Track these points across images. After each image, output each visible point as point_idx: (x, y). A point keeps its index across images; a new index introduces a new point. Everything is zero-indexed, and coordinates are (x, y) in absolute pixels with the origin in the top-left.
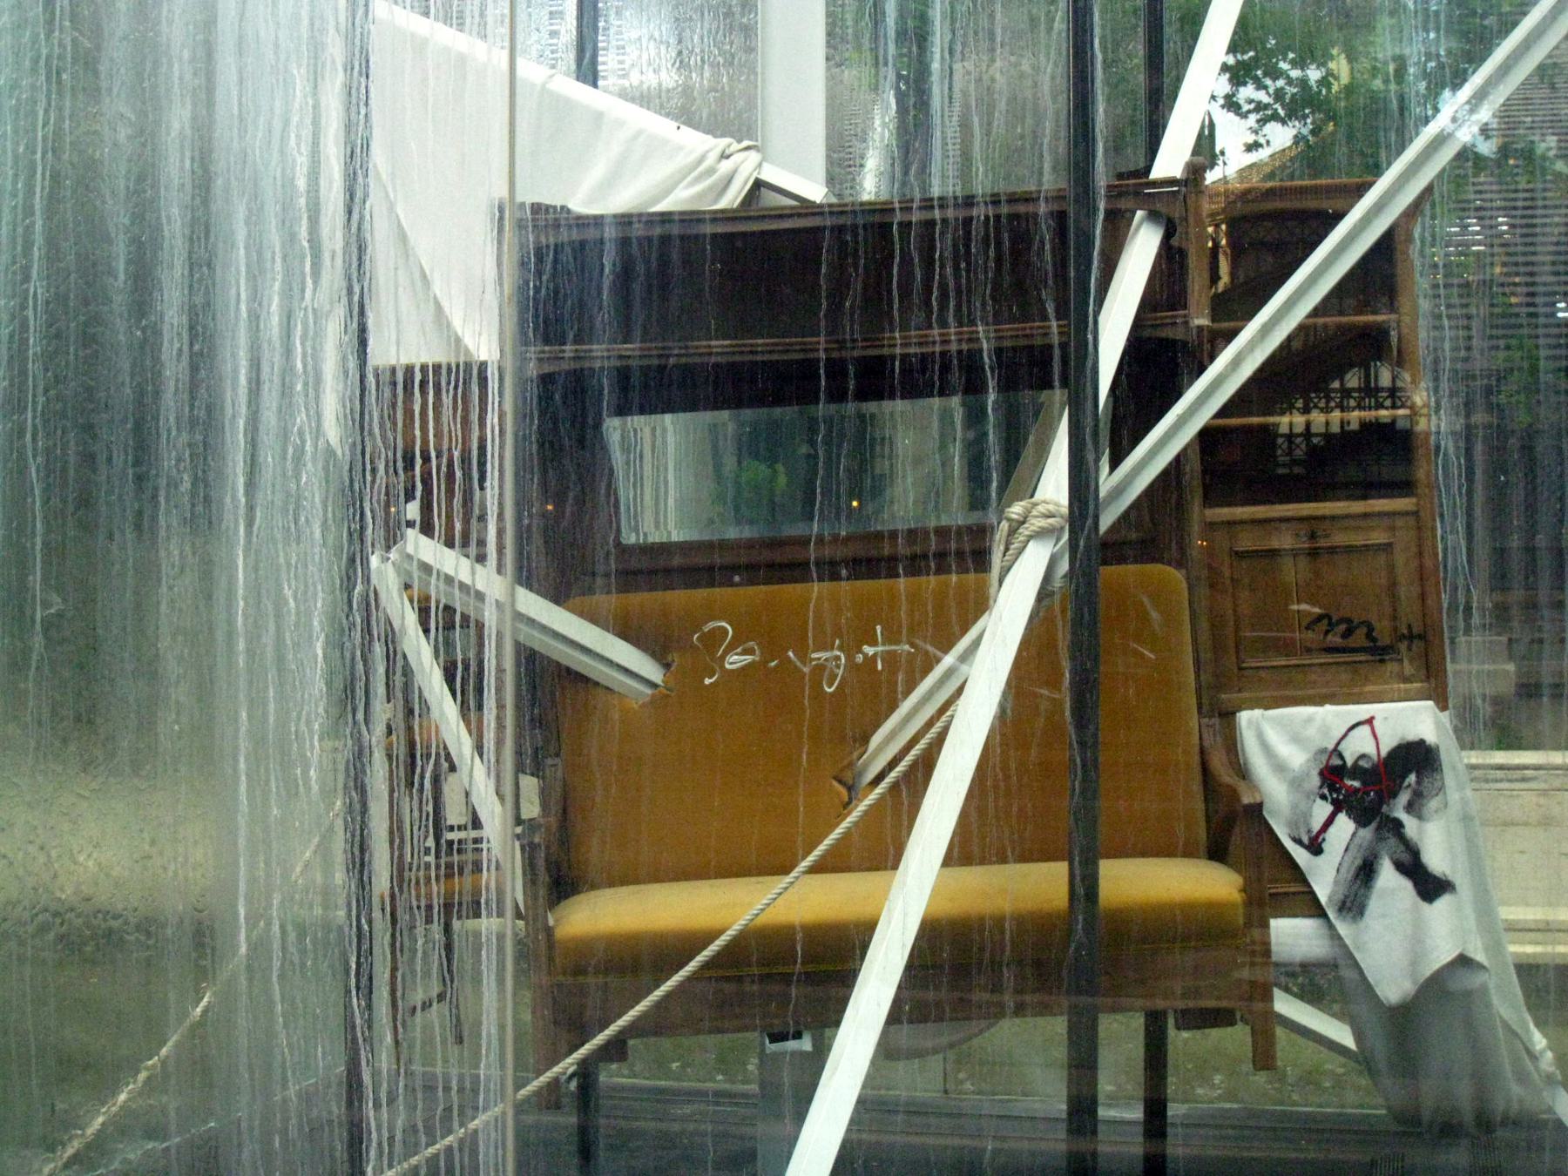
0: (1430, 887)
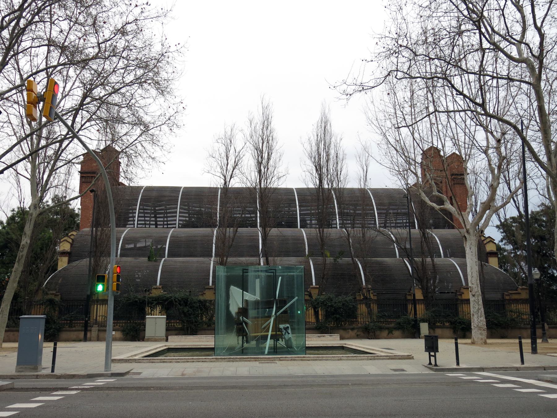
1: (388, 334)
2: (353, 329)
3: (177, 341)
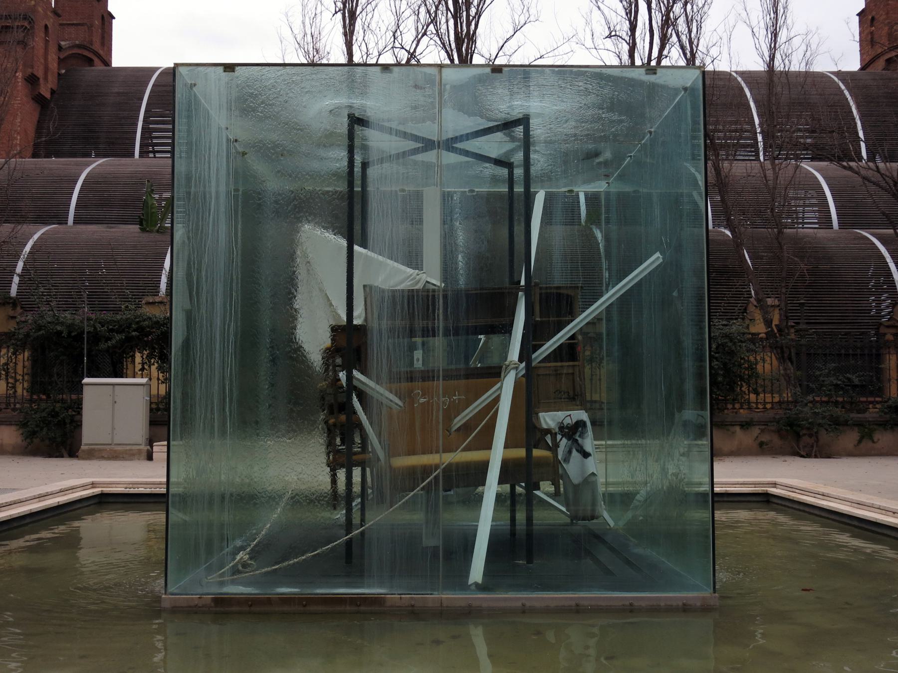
0: (586, 455)
1: (860, 442)
2: (746, 425)
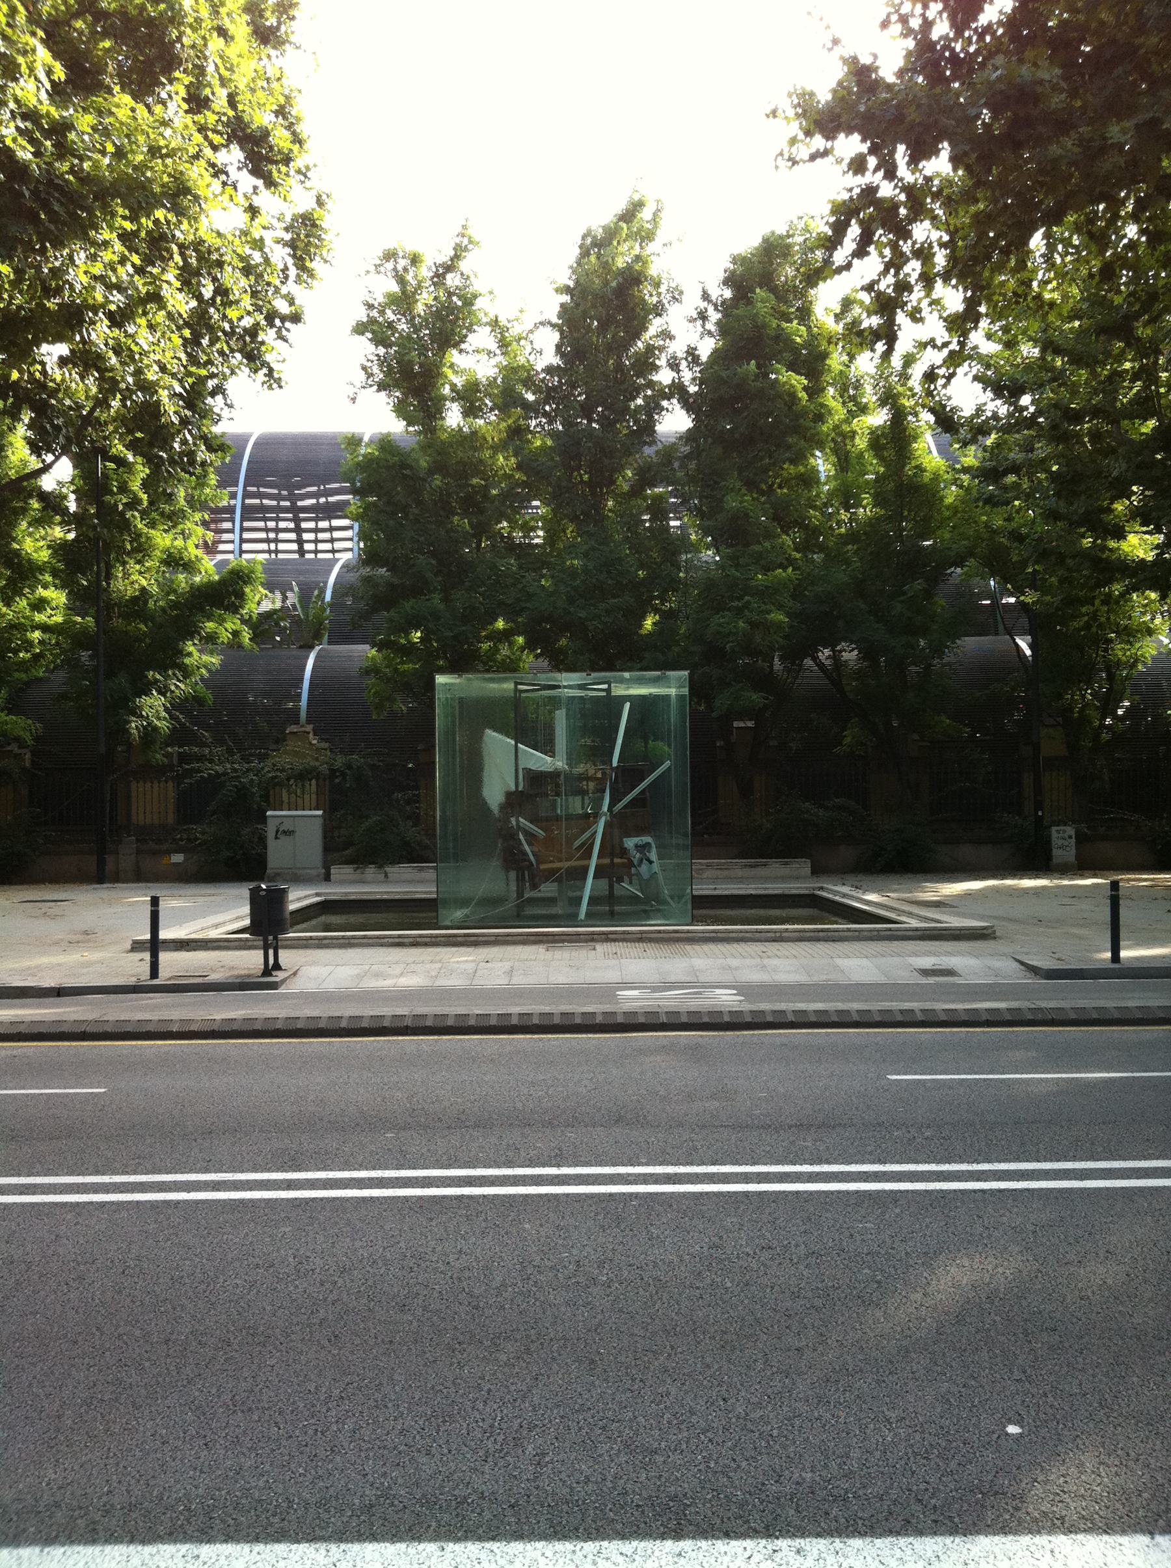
3: (348, 885)
